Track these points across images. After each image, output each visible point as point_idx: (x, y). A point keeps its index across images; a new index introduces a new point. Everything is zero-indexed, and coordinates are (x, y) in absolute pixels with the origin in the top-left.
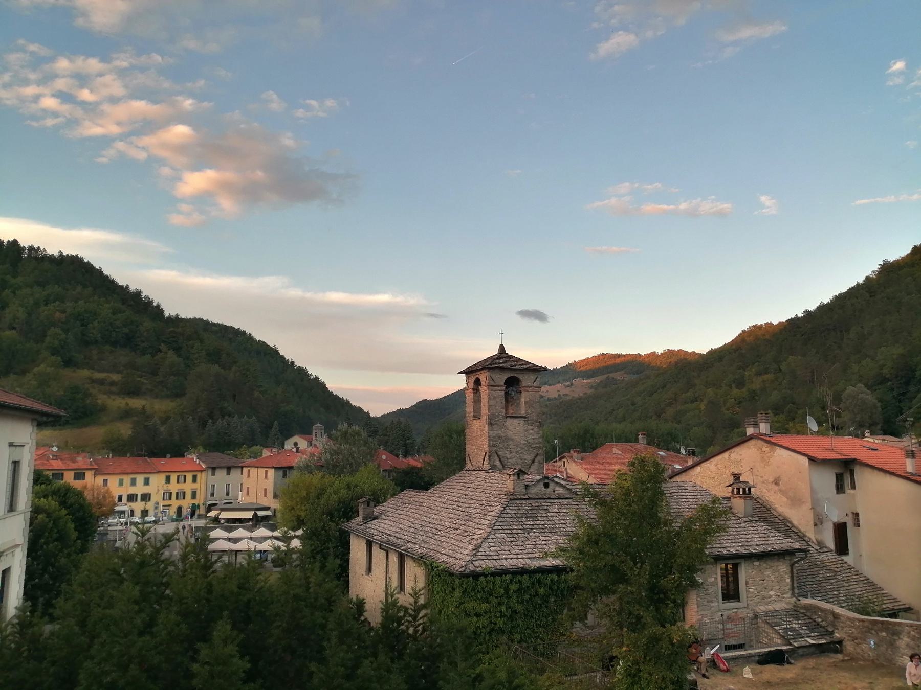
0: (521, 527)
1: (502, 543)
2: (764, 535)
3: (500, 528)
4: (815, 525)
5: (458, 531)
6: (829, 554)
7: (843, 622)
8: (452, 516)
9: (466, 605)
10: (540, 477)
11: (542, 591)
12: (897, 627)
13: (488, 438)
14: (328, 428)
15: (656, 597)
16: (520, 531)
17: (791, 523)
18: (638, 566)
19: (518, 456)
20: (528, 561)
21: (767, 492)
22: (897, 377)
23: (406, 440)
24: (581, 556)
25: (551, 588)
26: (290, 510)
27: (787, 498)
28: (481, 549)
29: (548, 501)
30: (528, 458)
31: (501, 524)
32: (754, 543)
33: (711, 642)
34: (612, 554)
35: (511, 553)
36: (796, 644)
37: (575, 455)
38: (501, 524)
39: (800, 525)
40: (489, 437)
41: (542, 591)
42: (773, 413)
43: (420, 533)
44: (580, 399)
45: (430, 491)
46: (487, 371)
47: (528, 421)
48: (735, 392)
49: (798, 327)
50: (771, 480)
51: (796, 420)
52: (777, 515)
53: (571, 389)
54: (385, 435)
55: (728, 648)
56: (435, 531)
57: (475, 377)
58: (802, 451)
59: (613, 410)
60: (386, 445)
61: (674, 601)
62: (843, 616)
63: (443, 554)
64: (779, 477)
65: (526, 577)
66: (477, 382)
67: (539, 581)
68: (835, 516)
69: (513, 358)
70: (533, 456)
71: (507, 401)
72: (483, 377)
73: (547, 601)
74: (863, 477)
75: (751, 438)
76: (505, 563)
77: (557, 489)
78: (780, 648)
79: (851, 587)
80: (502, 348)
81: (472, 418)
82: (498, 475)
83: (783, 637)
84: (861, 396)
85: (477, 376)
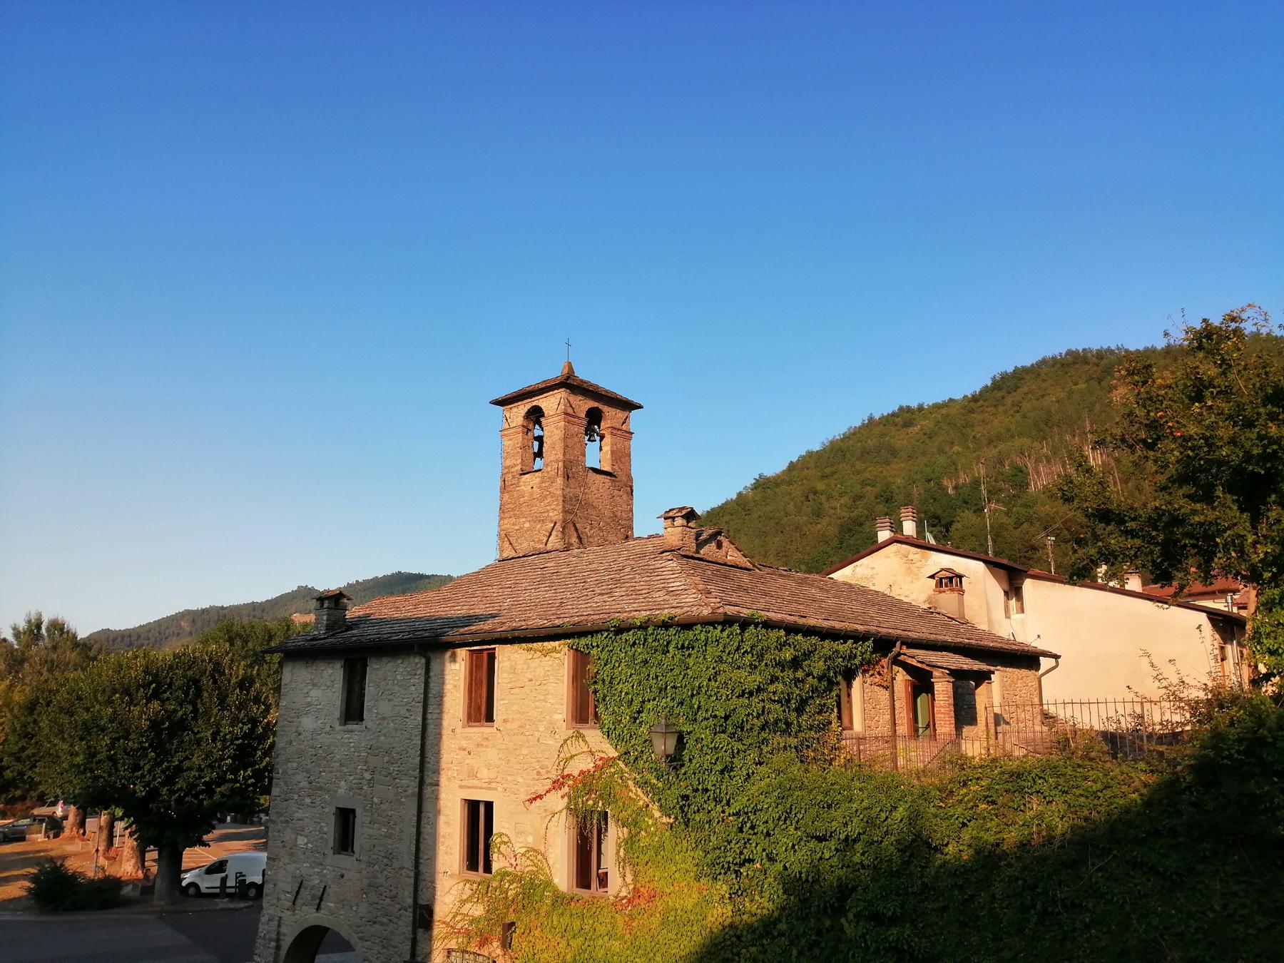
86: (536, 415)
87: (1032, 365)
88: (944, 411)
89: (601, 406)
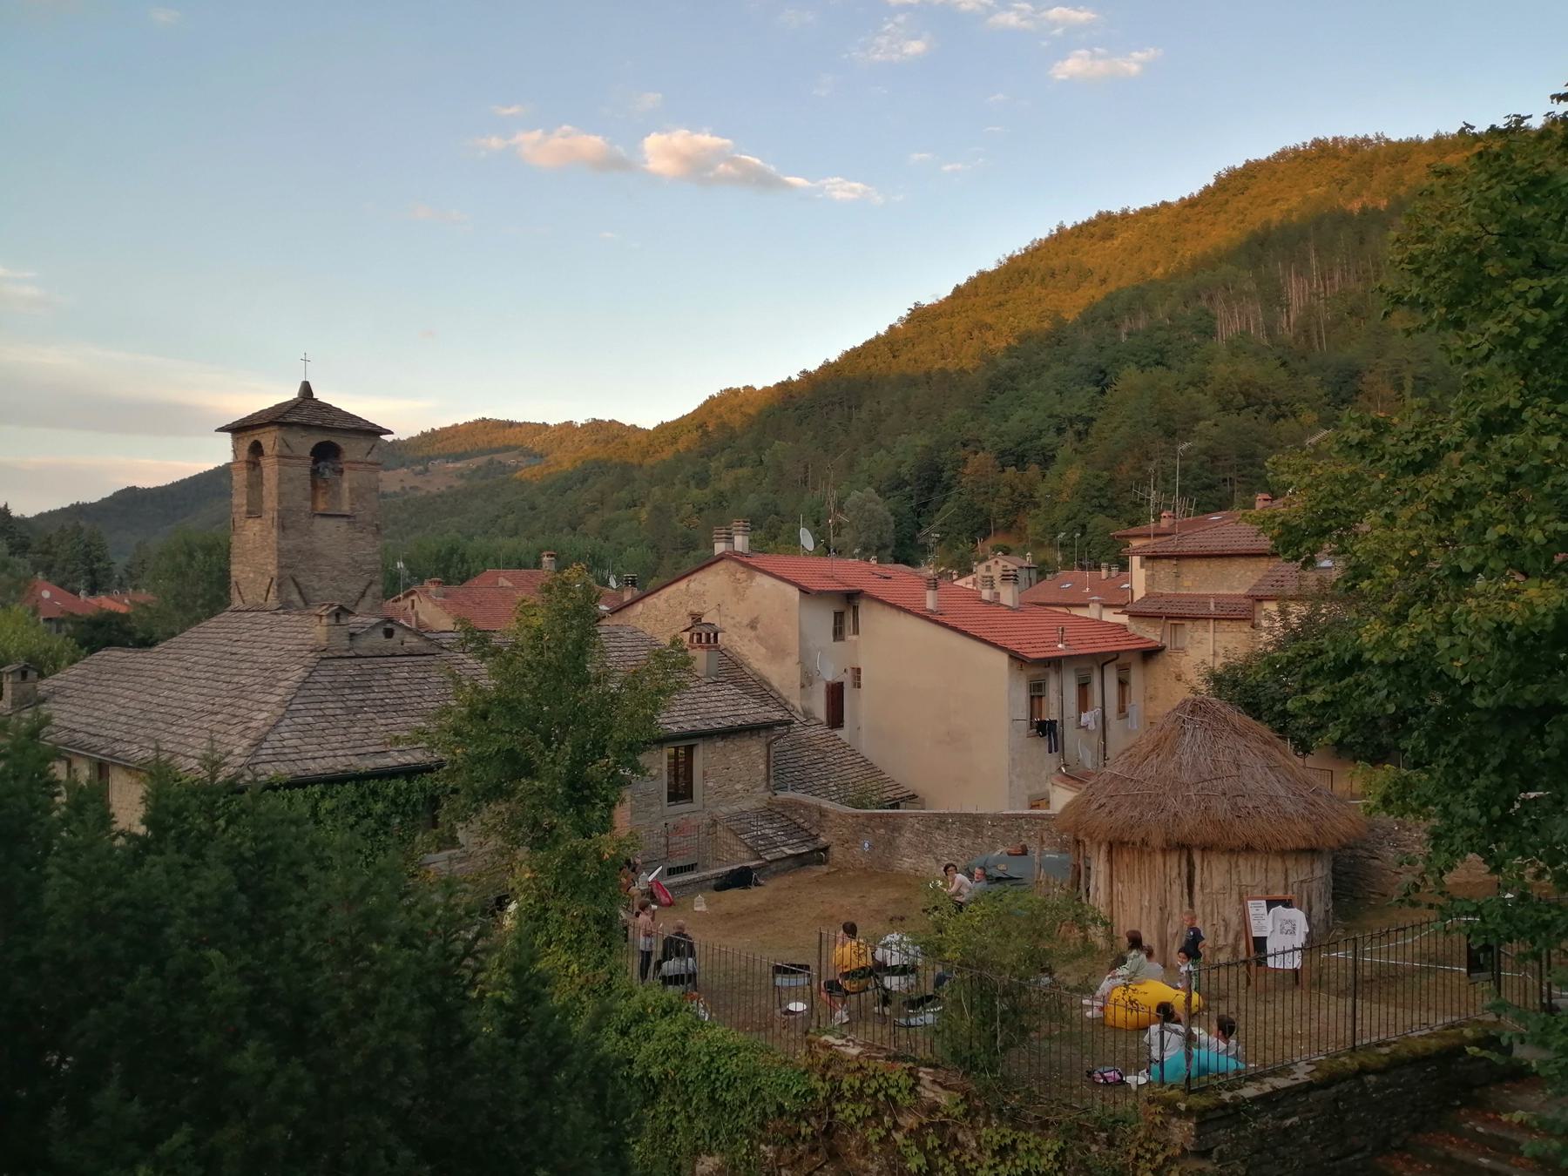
0: (341, 705)
1: (305, 731)
3: (301, 707)
4: (803, 686)
5: (220, 717)
6: (818, 727)
8: (205, 691)
10: (378, 620)
11: (379, 807)
12: (899, 821)
15: (576, 795)
16: (339, 711)
17: (769, 684)
18: (554, 746)
20: (354, 760)
22: (919, 479)
24: (458, 739)
25: (394, 802)
28: (265, 745)
29: (391, 659)
30: (355, 588)
31: (303, 700)
32: (718, 715)
33: (649, 866)
34: (510, 732)
35: (323, 749)
36: (768, 858)
37: (433, 588)
38: (303, 700)
40: (279, 550)
41: (379, 807)
43: (141, 723)
44: (439, 496)
45: (157, 649)
46: (275, 428)
47: (354, 523)
48: (695, 492)
50: (745, 622)
51: (779, 539)
54: (46, 553)
55: (672, 872)
56: (170, 719)
57: (252, 439)
58: (792, 578)
60: (48, 569)
61: (606, 799)
62: (833, 812)
63: (189, 757)
65: (350, 786)
66: (256, 449)
67: (374, 793)
68: (830, 673)
69: (327, 408)
70: (363, 584)
71: (314, 486)
72: (269, 439)
73: (387, 825)
74: (873, 619)
75: (721, 558)
76: (312, 765)
77: (408, 638)
78: (746, 865)
80: (306, 389)
81: (243, 515)
82: (297, 618)
83: (751, 848)
84: (870, 506)
85: (256, 438)
87: (1268, 159)
88: (1152, 219)
89: (333, 440)
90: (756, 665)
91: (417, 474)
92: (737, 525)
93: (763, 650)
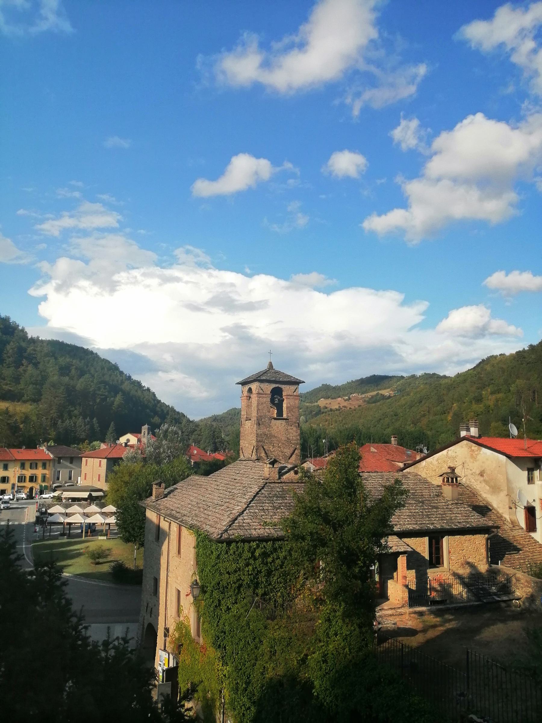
0: (271, 505)
2: (465, 514)
7: (522, 584)
9: (220, 565)
13: (256, 435)
14: (152, 431)
19: (280, 449)
21: (474, 481)
23: (215, 440)
26: (116, 492)
27: (489, 486)
29: (297, 484)
36: (485, 601)
39: (498, 507)
40: (257, 434)
42: (502, 423)
45: (210, 476)
48: (475, 406)
49: (524, 358)
50: (478, 472)
52: (482, 500)
53: (349, 402)
57: (249, 387)
58: (501, 450)
59: (380, 419)
64: (484, 470)
70: (292, 450)
72: (254, 386)
75: (464, 439)
76: (254, 532)
79: (535, 557)
80: (271, 365)
85: (250, 386)
86: (250, 390)
89: (280, 386)
90: (484, 495)
91: (345, 400)
92: (471, 423)
93: (488, 488)
